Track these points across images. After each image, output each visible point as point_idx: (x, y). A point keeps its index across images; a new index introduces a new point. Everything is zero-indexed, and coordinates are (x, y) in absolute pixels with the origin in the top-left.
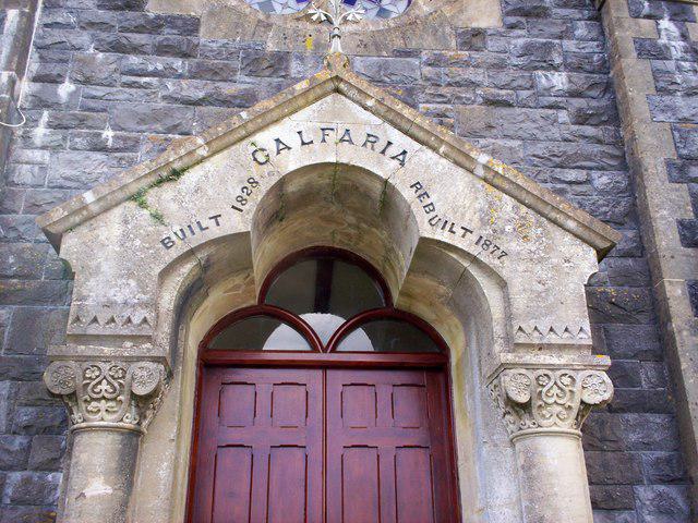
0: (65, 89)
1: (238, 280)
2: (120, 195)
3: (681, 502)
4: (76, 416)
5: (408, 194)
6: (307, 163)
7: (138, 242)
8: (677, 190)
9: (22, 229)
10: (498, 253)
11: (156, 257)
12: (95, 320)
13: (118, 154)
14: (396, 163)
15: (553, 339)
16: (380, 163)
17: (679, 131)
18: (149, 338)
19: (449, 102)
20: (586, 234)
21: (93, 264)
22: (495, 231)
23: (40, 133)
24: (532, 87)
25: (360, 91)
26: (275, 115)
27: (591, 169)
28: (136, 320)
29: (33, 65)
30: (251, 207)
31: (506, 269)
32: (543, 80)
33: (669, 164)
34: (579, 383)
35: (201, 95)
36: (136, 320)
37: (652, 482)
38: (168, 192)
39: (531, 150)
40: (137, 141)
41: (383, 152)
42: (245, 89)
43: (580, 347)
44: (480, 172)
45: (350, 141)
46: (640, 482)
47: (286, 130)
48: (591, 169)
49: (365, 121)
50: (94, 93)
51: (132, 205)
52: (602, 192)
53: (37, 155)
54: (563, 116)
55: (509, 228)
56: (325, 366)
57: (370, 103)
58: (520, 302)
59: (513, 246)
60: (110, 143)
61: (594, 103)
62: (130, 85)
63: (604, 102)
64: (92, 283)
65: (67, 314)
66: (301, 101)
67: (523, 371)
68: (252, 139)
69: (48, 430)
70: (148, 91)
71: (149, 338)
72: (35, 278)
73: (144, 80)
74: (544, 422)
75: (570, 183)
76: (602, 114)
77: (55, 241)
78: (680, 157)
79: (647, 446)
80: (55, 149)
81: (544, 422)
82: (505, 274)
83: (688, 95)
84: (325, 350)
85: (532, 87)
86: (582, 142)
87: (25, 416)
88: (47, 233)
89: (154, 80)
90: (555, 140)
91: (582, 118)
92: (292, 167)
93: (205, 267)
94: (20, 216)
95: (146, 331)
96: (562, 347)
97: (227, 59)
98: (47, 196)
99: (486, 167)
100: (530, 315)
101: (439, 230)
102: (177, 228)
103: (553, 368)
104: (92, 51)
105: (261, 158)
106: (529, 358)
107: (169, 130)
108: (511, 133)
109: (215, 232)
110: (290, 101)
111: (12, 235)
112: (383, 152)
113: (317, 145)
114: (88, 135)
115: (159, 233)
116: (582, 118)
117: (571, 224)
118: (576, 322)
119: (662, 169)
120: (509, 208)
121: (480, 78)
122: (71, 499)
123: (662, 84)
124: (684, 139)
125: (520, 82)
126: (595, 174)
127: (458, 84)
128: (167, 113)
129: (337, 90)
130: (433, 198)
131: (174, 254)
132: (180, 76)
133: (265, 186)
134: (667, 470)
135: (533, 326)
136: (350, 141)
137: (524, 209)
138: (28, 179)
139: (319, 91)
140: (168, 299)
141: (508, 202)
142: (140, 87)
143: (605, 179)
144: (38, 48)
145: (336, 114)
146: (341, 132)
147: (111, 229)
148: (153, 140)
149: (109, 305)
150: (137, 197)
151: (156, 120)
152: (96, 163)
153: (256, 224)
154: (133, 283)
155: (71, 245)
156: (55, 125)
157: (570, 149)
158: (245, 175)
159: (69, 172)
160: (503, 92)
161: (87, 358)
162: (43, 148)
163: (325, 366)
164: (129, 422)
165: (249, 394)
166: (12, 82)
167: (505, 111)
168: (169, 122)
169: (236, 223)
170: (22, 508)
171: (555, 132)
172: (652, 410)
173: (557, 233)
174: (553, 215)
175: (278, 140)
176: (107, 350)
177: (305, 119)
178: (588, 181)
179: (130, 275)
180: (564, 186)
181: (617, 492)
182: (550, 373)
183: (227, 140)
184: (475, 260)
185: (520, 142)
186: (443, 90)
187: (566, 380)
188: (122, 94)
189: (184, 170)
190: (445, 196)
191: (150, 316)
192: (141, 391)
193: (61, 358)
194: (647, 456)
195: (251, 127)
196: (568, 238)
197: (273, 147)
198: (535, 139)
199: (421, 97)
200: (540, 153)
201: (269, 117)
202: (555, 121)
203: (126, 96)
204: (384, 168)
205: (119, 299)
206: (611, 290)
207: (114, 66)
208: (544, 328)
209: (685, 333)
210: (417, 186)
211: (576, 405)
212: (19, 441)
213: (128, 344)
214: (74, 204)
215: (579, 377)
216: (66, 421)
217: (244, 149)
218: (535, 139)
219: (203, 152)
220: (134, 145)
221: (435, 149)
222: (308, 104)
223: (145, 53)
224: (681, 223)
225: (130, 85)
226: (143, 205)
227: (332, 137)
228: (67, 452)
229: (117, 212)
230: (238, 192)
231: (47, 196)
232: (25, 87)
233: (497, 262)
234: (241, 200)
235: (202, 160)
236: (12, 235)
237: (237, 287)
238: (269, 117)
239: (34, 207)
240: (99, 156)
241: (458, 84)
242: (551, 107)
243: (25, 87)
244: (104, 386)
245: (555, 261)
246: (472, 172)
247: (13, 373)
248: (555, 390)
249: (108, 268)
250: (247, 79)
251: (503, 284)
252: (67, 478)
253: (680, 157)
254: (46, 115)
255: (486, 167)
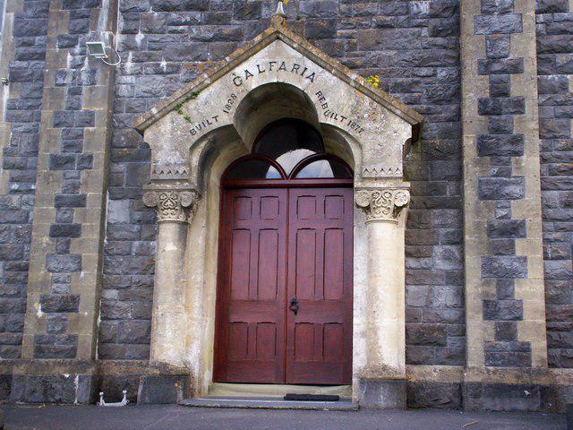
0: (139, 37)
1: (235, 144)
2: (169, 108)
3: (457, 254)
4: (159, 216)
5: (314, 99)
6: (261, 84)
7: (179, 132)
8: (482, 80)
9: (126, 122)
10: (359, 129)
11: (188, 140)
12: (162, 172)
13: (169, 76)
14: (308, 81)
15: (383, 174)
16: (300, 81)
17: (490, 41)
18: (187, 180)
19: (355, 28)
20: (406, 117)
21: (159, 144)
22: (358, 117)
23: (129, 65)
24: (407, 13)
25: (290, 39)
26: (244, 57)
27: (437, 66)
28: (181, 172)
29: (121, 24)
30: (233, 110)
31: (362, 138)
32: (415, 8)
33: (480, 63)
34: (393, 196)
35: (211, 35)
36: (181, 172)
37: (443, 244)
38: (192, 104)
39: (402, 56)
40: (178, 67)
41: (302, 75)
42: (236, 30)
43: (396, 178)
44: (353, 84)
45: (285, 69)
46: (437, 244)
47: (250, 65)
48: (437, 66)
49: (291, 54)
50: (154, 39)
51: (175, 113)
52: (441, 82)
53: (128, 79)
54: (425, 32)
55: (366, 115)
56: (288, 187)
57: (295, 46)
58: (368, 155)
59: (368, 125)
60: (165, 69)
61: (445, 22)
62: (173, 32)
63: (452, 20)
64: (159, 154)
65: (149, 170)
66: (258, 48)
67: (366, 191)
68: (233, 71)
69: (148, 222)
70: (183, 35)
71: (187, 180)
72: (135, 147)
73: (181, 27)
74: (375, 215)
75: (423, 77)
76: (448, 30)
77: (142, 132)
78: (488, 57)
79: (443, 226)
80: (138, 74)
81: (375, 215)
82: (361, 141)
83: (503, 14)
84: (287, 178)
85: (407, 13)
86: (434, 49)
87: (137, 216)
88: (137, 130)
89: (186, 27)
90: (417, 48)
91: (436, 33)
92: (254, 87)
93: (214, 142)
94: (124, 114)
95: (185, 177)
96: (387, 179)
97: (225, 10)
98: (136, 103)
99: (355, 81)
100: (372, 162)
101: (329, 119)
102: (197, 124)
103: (381, 189)
104: (151, 12)
105: (238, 83)
106: (369, 184)
107: (196, 59)
108: (391, 46)
109: (216, 125)
110: (251, 48)
111: (121, 125)
112: (302, 75)
113: (267, 73)
114: (154, 65)
115: (188, 127)
116: (436, 33)
117: (398, 112)
118: (396, 165)
119: (475, 67)
120: (368, 104)
121: (375, 10)
122: (160, 252)
123: (485, 8)
124: (492, 45)
125: (400, 10)
126: (439, 70)
127: (361, 15)
128: (194, 48)
129: (278, 38)
130: (327, 100)
131: (196, 138)
132: (199, 24)
133: (240, 97)
134: (452, 238)
135: (376, 169)
136: (285, 69)
137: (375, 104)
138: (126, 93)
139: (268, 41)
140: (195, 160)
141: (367, 100)
142: (179, 33)
143: (444, 73)
144: (122, 12)
145: (278, 53)
146: (280, 64)
147: (166, 125)
148: (187, 66)
149: (168, 165)
150: (177, 108)
151: (188, 53)
152: (158, 83)
153: (237, 117)
154: (178, 153)
155: (149, 136)
156: (136, 61)
157: (425, 54)
158: (230, 93)
159: (145, 88)
160: (389, 18)
161: (160, 190)
162: (132, 74)
163: (288, 187)
164: (182, 219)
165: (258, 208)
166: (111, 38)
167: (388, 31)
168: (196, 54)
169: (226, 119)
170: (141, 257)
171: (418, 43)
172: (449, 207)
173: (392, 117)
174: (389, 107)
175: (246, 71)
176: (169, 186)
177: (260, 58)
178: (434, 75)
179: (176, 150)
180: (418, 79)
181: (423, 249)
182: (391, 192)
183: (222, 72)
184: (347, 134)
185: (395, 52)
186: (352, 20)
187: (387, 195)
188: (168, 37)
189: (199, 92)
190: (334, 98)
191: (187, 169)
192: (185, 205)
193: (150, 190)
194: (443, 231)
195: (232, 65)
196: (397, 119)
197: (243, 75)
198: (405, 49)
199: (339, 25)
200: (406, 58)
201: (241, 59)
202: (419, 35)
203: (172, 39)
204: (301, 84)
205: (172, 162)
206: (437, 142)
207: (163, 21)
208: (378, 169)
209: (470, 166)
210: (319, 93)
211: (392, 207)
212: (136, 227)
213: (178, 183)
214: (148, 115)
215: (394, 193)
216: (156, 219)
217: (229, 77)
218: (405, 49)
219: (208, 82)
220: (176, 69)
221: (330, 72)
222: (262, 48)
223: (179, 10)
224: (480, 101)
225: (173, 32)
226: (180, 113)
227: (275, 67)
228: (157, 233)
229: (168, 116)
230: (226, 102)
231: (136, 103)
232: (119, 38)
233: (358, 135)
234: (228, 106)
235: (208, 85)
236: (121, 125)
237: (236, 147)
238: (241, 59)
239: (130, 109)
240: (160, 78)
241: (361, 15)
242: (418, 26)
243: (119, 38)
244: (169, 203)
245: (389, 132)
246: (348, 83)
247: (130, 196)
248: (382, 200)
249: (166, 146)
250: (238, 22)
251: (361, 146)
252: (158, 244)
253: (488, 57)
254: (131, 55)
255: (355, 81)
